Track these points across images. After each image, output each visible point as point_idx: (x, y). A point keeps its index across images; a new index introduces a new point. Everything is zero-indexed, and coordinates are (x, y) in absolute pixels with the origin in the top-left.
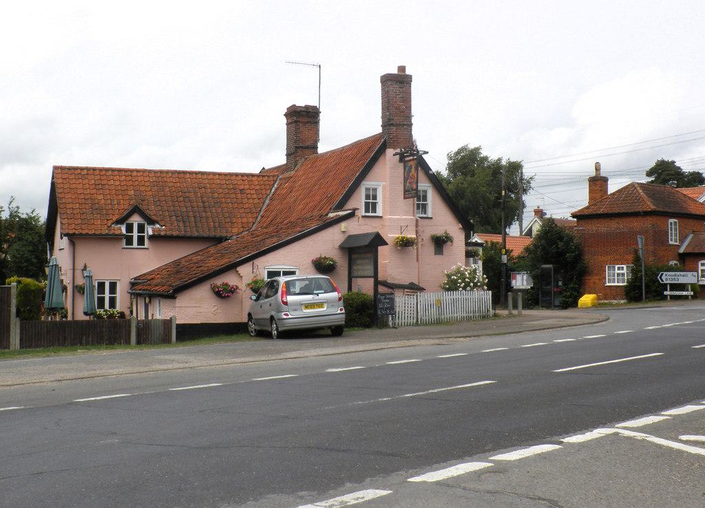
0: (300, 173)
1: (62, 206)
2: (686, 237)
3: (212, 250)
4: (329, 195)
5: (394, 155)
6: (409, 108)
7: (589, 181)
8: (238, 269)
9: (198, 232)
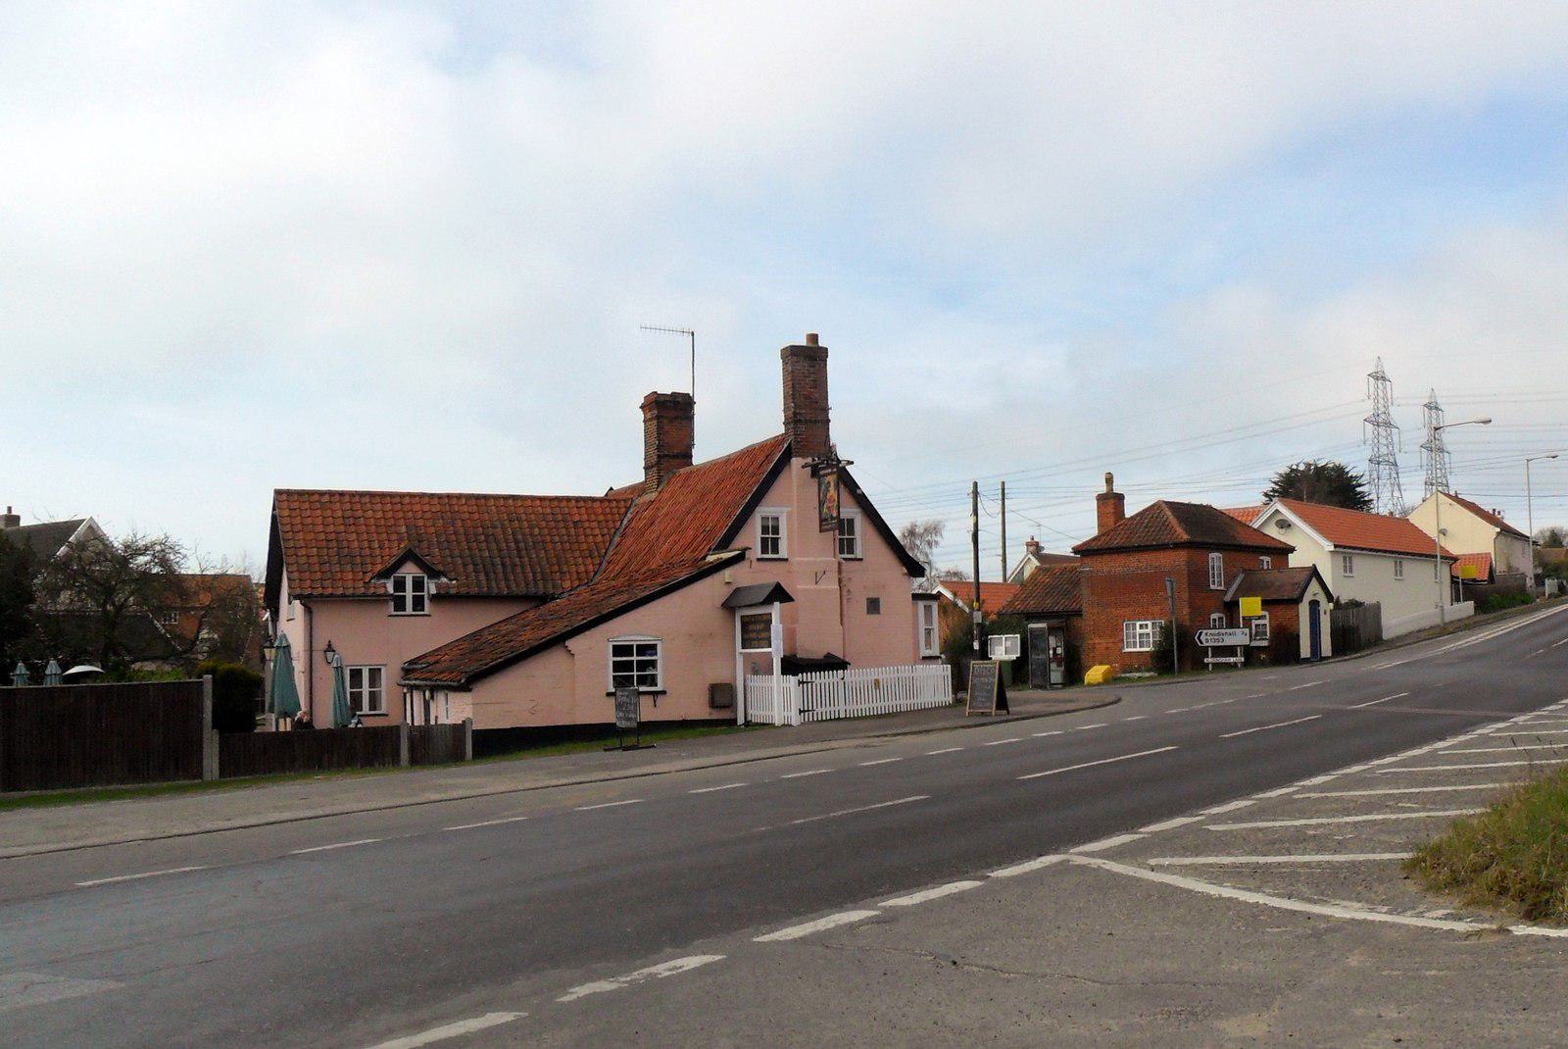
0: (666, 496)
2: (1235, 577)
4: (708, 529)
5: (803, 467)
7: (1098, 500)
8: (567, 643)
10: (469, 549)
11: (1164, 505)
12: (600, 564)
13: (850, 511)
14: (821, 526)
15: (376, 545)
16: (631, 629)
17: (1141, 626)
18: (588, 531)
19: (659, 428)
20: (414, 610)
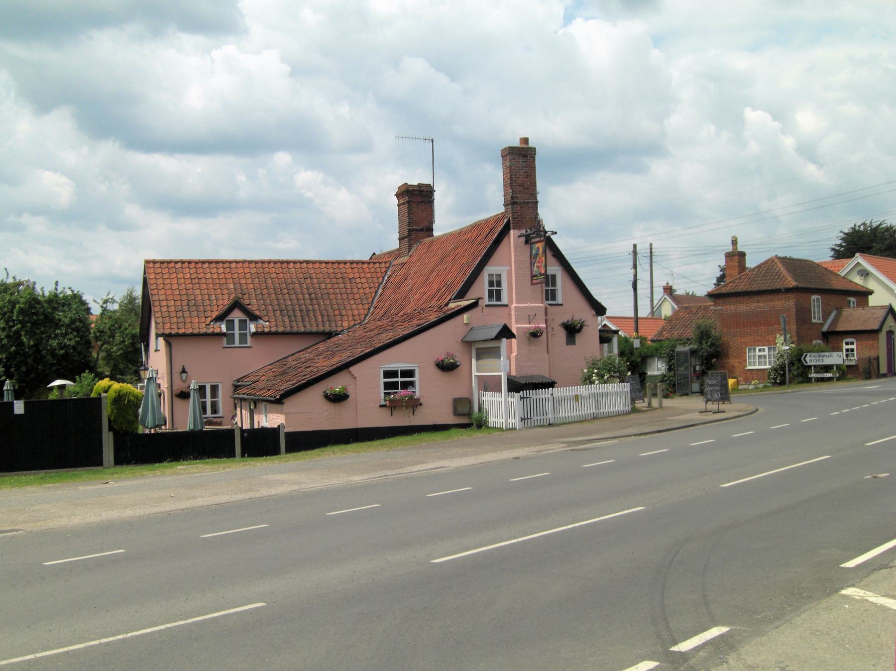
0: (415, 259)
1: (157, 303)
2: (829, 314)
3: (322, 347)
4: (448, 283)
5: (519, 237)
6: (534, 184)
7: (726, 257)
9: (305, 327)
10: (277, 299)
11: (777, 261)
12: (369, 309)
13: (555, 269)
14: (532, 280)
15: (213, 297)
16: (395, 359)
17: (760, 350)
18: (360, 285)
19: (409, 210)
20: (227, 344)
